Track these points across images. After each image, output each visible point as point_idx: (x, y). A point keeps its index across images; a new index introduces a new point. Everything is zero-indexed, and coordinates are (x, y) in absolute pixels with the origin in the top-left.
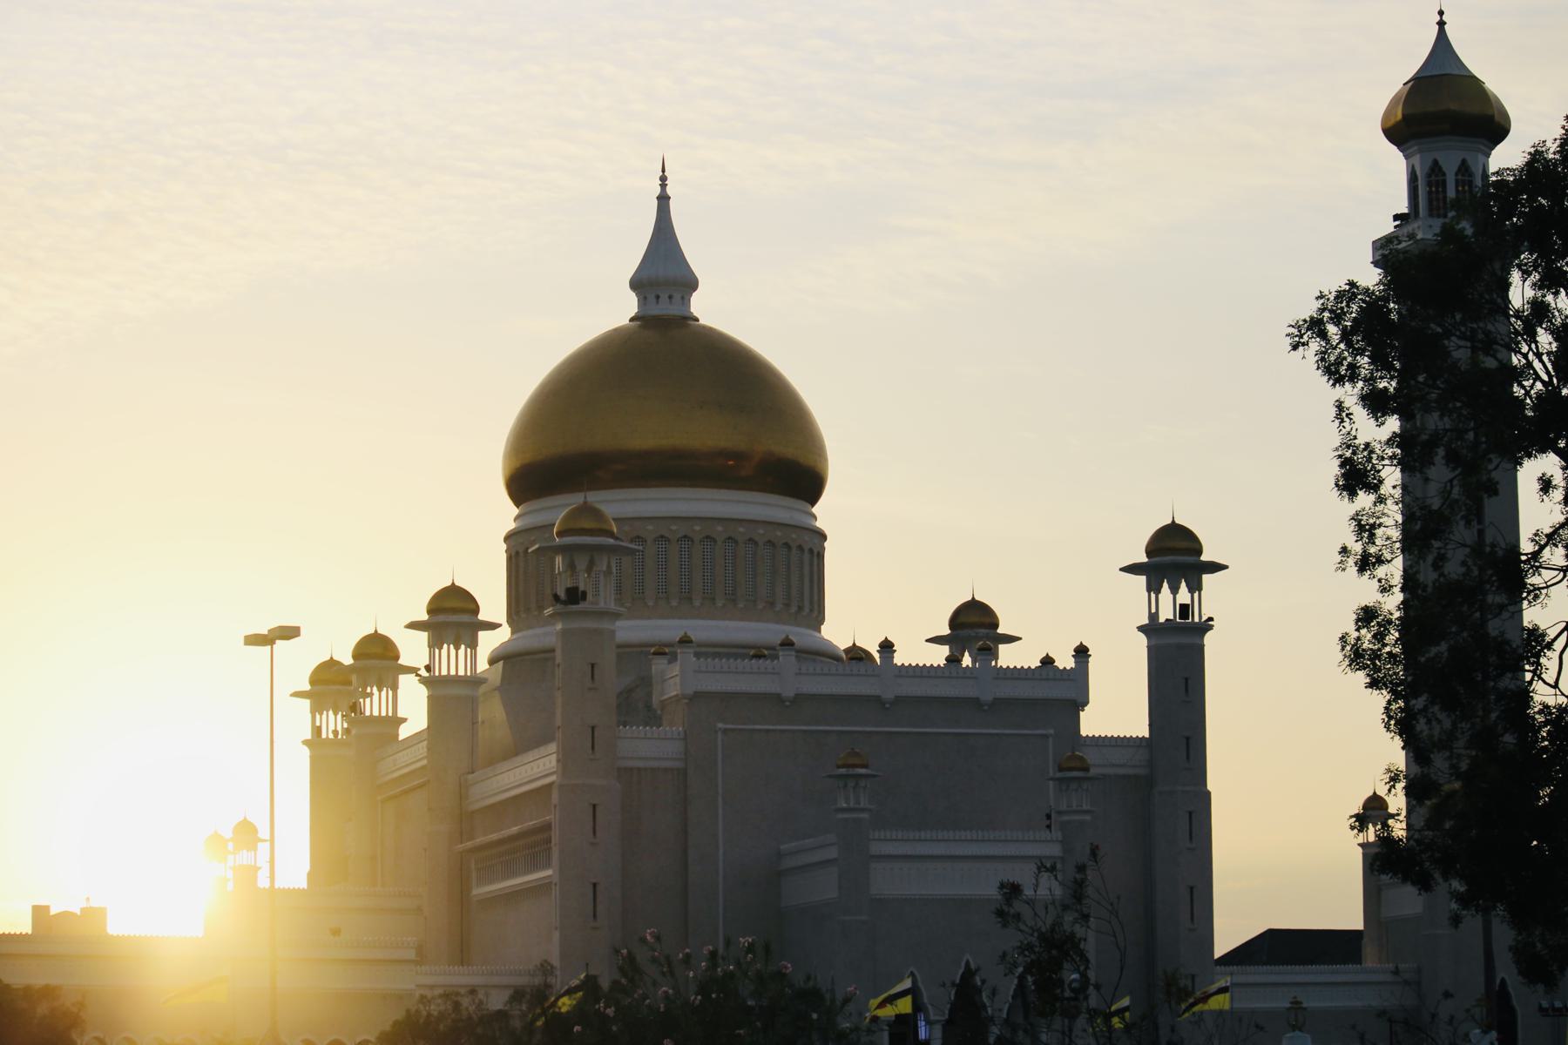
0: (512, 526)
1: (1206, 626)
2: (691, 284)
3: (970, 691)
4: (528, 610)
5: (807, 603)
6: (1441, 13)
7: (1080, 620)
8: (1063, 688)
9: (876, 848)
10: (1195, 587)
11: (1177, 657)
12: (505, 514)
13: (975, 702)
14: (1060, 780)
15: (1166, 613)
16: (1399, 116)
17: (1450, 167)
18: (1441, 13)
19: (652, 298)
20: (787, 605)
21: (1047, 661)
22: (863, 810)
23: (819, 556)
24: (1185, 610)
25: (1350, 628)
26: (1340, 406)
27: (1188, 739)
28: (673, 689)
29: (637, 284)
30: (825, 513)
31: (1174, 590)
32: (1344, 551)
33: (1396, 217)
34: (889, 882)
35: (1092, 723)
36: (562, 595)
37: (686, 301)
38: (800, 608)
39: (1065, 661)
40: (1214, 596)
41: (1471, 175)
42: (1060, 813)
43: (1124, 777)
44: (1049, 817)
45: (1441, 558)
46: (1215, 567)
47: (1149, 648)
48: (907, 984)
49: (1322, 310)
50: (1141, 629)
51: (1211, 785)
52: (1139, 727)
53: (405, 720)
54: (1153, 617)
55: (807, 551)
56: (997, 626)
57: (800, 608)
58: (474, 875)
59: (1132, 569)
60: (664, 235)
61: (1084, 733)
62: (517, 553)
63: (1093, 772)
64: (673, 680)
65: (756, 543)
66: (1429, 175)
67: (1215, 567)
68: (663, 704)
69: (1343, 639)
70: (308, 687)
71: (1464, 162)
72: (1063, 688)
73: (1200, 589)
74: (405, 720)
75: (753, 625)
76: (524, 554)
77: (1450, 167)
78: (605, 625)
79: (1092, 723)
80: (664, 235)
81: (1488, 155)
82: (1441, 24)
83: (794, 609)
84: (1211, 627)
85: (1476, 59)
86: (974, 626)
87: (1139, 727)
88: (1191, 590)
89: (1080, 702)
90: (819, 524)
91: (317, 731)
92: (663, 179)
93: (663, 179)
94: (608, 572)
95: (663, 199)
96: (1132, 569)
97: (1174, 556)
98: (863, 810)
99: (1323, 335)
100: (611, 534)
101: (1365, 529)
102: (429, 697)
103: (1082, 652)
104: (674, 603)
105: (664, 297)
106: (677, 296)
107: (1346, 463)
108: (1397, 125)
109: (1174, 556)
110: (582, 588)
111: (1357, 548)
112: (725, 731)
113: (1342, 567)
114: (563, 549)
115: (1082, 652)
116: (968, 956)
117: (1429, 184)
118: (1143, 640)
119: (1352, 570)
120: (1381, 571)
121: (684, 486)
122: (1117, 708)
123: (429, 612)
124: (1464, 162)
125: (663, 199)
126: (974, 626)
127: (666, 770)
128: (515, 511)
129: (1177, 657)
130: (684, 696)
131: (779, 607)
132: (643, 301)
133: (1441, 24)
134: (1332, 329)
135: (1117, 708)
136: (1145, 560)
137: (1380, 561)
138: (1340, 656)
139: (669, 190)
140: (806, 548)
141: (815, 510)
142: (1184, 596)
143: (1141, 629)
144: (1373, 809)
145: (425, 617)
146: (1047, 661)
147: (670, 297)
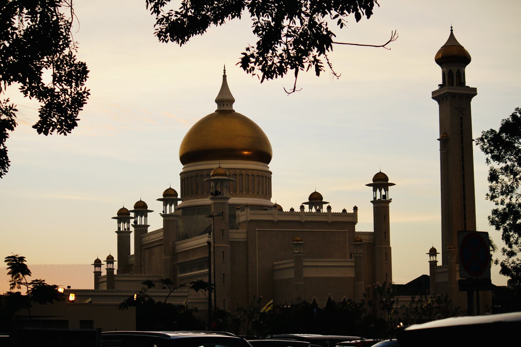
0: (182, 171)
1: (390, 201)
2: (232, 101)
3: (325, 219)
4: (188, 195)
5: (261, 190)
6: (452, 27)
7: (349, 196)
8: (349, 219)
9: (305, 264)
10: (386, 190)
11: (381, 209)
12: (180, 168)
13: (327, 222)
14: (354, 245)
15: (378, 197)
16: (440, 56)
17: (455, 71)
18: (452, 27)
19: (222, 105)
20: (263, 193)
21: (344, 211)
22: (301, 253)
23: (270, 179)
24: (384, 197)
25: (490, 214)
26: (487, 159)
27: (223, 252)
28: (242, 219)
29: (217, 101)
30: (272, 166)
31: (380, 191)
32: (487, 195)
33: (439, 85)
34: (308, 273)
35: (358, 228)
36: (214, 193)
37: (231, 106)
38: (266, 194)
39: (350, 211)
40: (392, 193)
41: (460, 73)
42: (354, 254)
43: (367, 243)
44: (351, 255)
45: (512, 197)
46: (392, 184)
47: (374, 207)
48: (272, 301)
49: (483, 135)
50: (371, 202)
51: (391, 245)
52: (371, 229)
54: (375, 198)
55: (267, 177)
56: (322, 199)
57: (266, 194)
58: (178, 271)
59: (369, 185)
61: (356, 230)
62: (185, 178)
63: (363, 241)
64: (242, 216)
65: (254, 176)
66: (448, 74)
67: (392, 184)
68: (239, 223)
69: (489, 217)
70: (116, 216)
71: (458, 70)
72: (349, 219)
73: (388, 191)
76: (185, 178)
77: (455, 71)
78: (226, 201)
79: (358, 228)
81: (465, 68)
82: (452, 30)
83: (264, 194)
84: (391, 201)
85: (461, 40)
86: (316, 199)
87: (371, 229)
88: (385, 191)
89: (355, 222)
90: (270, 170)
91: (119, 228)
92: (225, 70)
93: (225, 70)
94: (226, 186)
95: (225, 77)
96: (369, 185)
97: (381, 182)
98: (301, 253)
99: (484, 141)
100: (227, 176)
101: (492, 189)
103: (355, 208)
104: (231, 193)
105: (225, 104)
106: (229, 105)
107: (490, 174)
108: (439, 59)
109: (381, 182)
110: (219, 191)
111: (490, 194)
112: (258, 231)
113: (487, 199)
114: (215, 181)
115: (355, 208)
116: (330, 293)
117: (449, 76)
118: (372, 205)
119: (489, 199)
120: (496, 200)
121: (233, 159)
122: (365, 224)
123: (163, 196)
124: (458, 70)
125: (225, 77)
126: (316, 199)
127: (242, 242)
128: (183, 166)
129: (381, 209)
130: (247, 221)
131: (260, 194)
133: (452, 30)
134: (486, 140)
135: (365, 224)
136: (372, 182)
137: (496, 197)
138: (488, 222)
140: (256, 175)
141: (269, 165)
142: (383, 193)
143: (371, 202)
144: (433, 251)
145: (162, 197)
146: (344, 211)
147: (224, 105)
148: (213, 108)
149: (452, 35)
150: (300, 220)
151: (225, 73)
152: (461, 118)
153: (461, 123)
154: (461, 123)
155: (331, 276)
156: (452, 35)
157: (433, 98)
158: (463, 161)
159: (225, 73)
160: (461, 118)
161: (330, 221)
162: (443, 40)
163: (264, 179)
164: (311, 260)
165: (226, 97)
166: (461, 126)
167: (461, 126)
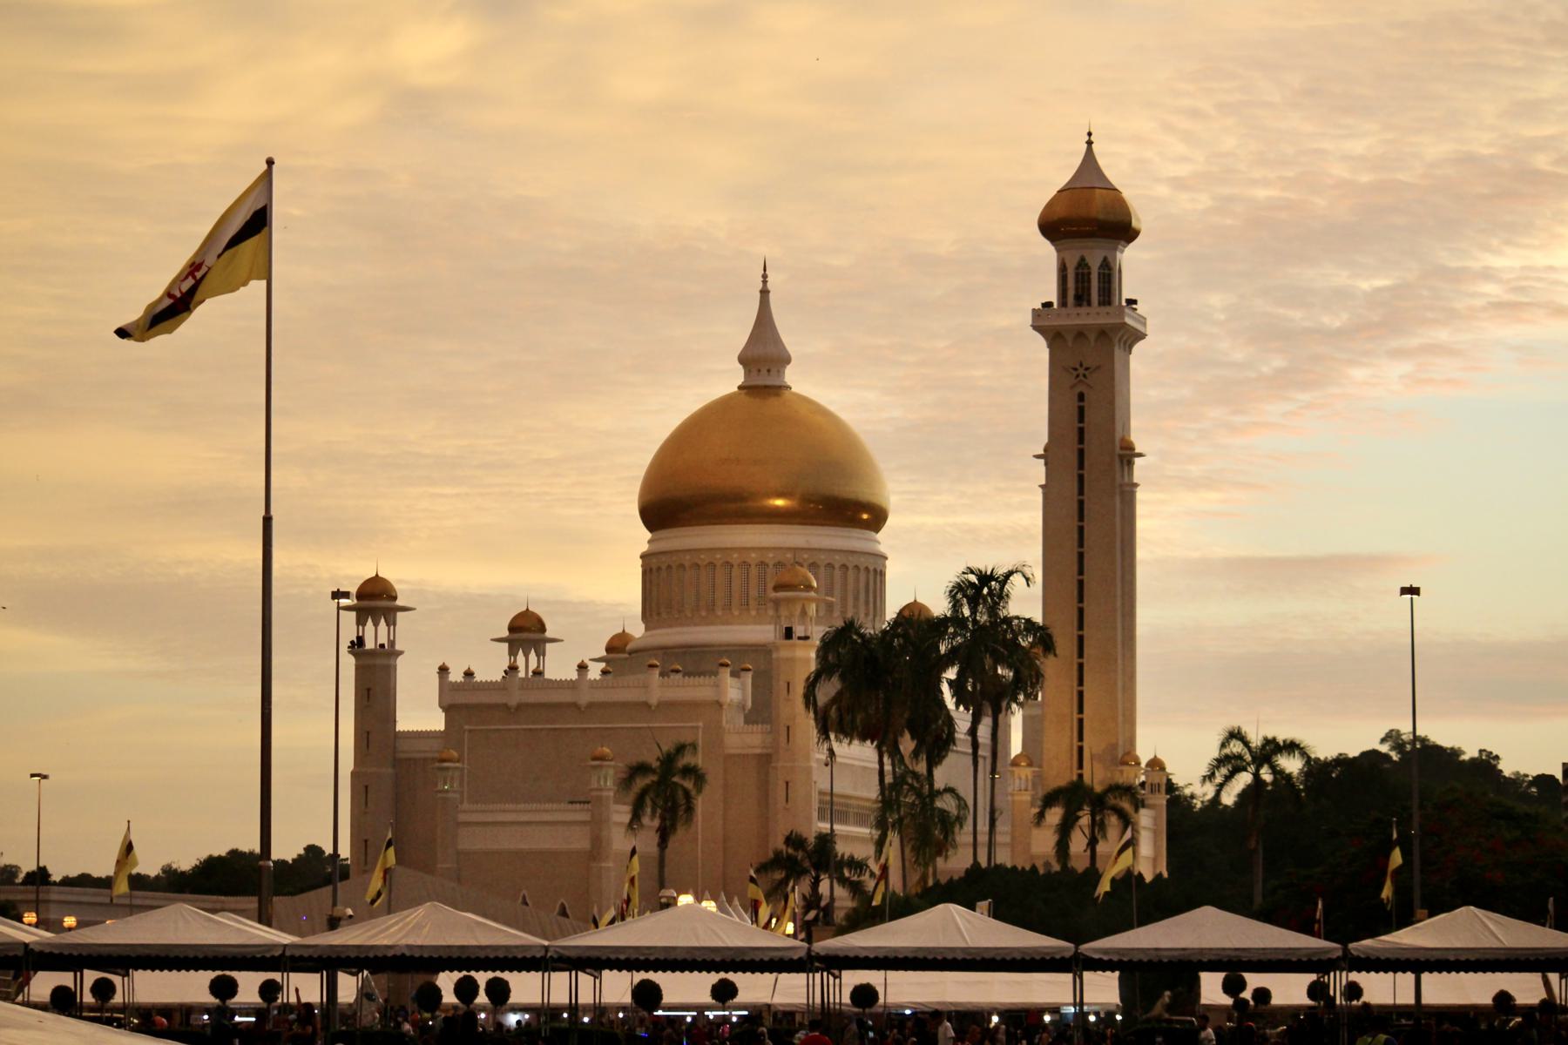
6: (1090, 134)
9: (462, 817)
17: (1095, 265)
18: (1090, 134)
19: (764, 371)
29: (743, 360)
30: (885, 540)
34: (1428, 998)
37: (780, 373)
41: (1110, 269)
43: (755, 755)
53: (401, 653)
60: (764, 323)
74: (401, 653)
75: (758, 627)
77: (1095, 265)
80: (764, 323)
82: (1090, 143)
85: (1115, 169)
92: (765, 276)
95: (765, 293)
102: (1455, 753)
105: (764, 371)
106: (774, 372)
116: (524, 892)
124: (1105, 259)
125: (765, 293)
128: (648, 535)
132: (748, 373)
133: (1090, 143)
139: (769, 286)
140: (850, 566)
148: (728, 380)
149: (1089, 156)
150: (643, 699)
151: (765, 282)
152: (1081, 397)
153: (1081, 411)
154: (1081, 411)
155: (524, 846)
156: (1089, 156)
157: (1035, 328)
158: (1081, 518)
159: (765, 282)
160: (1081, 397)
161: (654, 701)
162: (1059, 174)
163: (851, 573)
164: (483, 807)
165: (1093, 316)
166: (1081, 419)
167: (1081, 419)
